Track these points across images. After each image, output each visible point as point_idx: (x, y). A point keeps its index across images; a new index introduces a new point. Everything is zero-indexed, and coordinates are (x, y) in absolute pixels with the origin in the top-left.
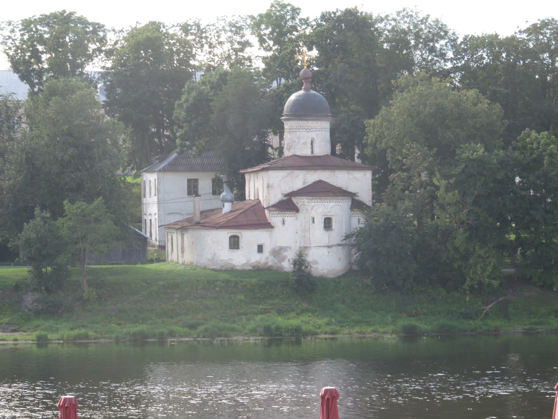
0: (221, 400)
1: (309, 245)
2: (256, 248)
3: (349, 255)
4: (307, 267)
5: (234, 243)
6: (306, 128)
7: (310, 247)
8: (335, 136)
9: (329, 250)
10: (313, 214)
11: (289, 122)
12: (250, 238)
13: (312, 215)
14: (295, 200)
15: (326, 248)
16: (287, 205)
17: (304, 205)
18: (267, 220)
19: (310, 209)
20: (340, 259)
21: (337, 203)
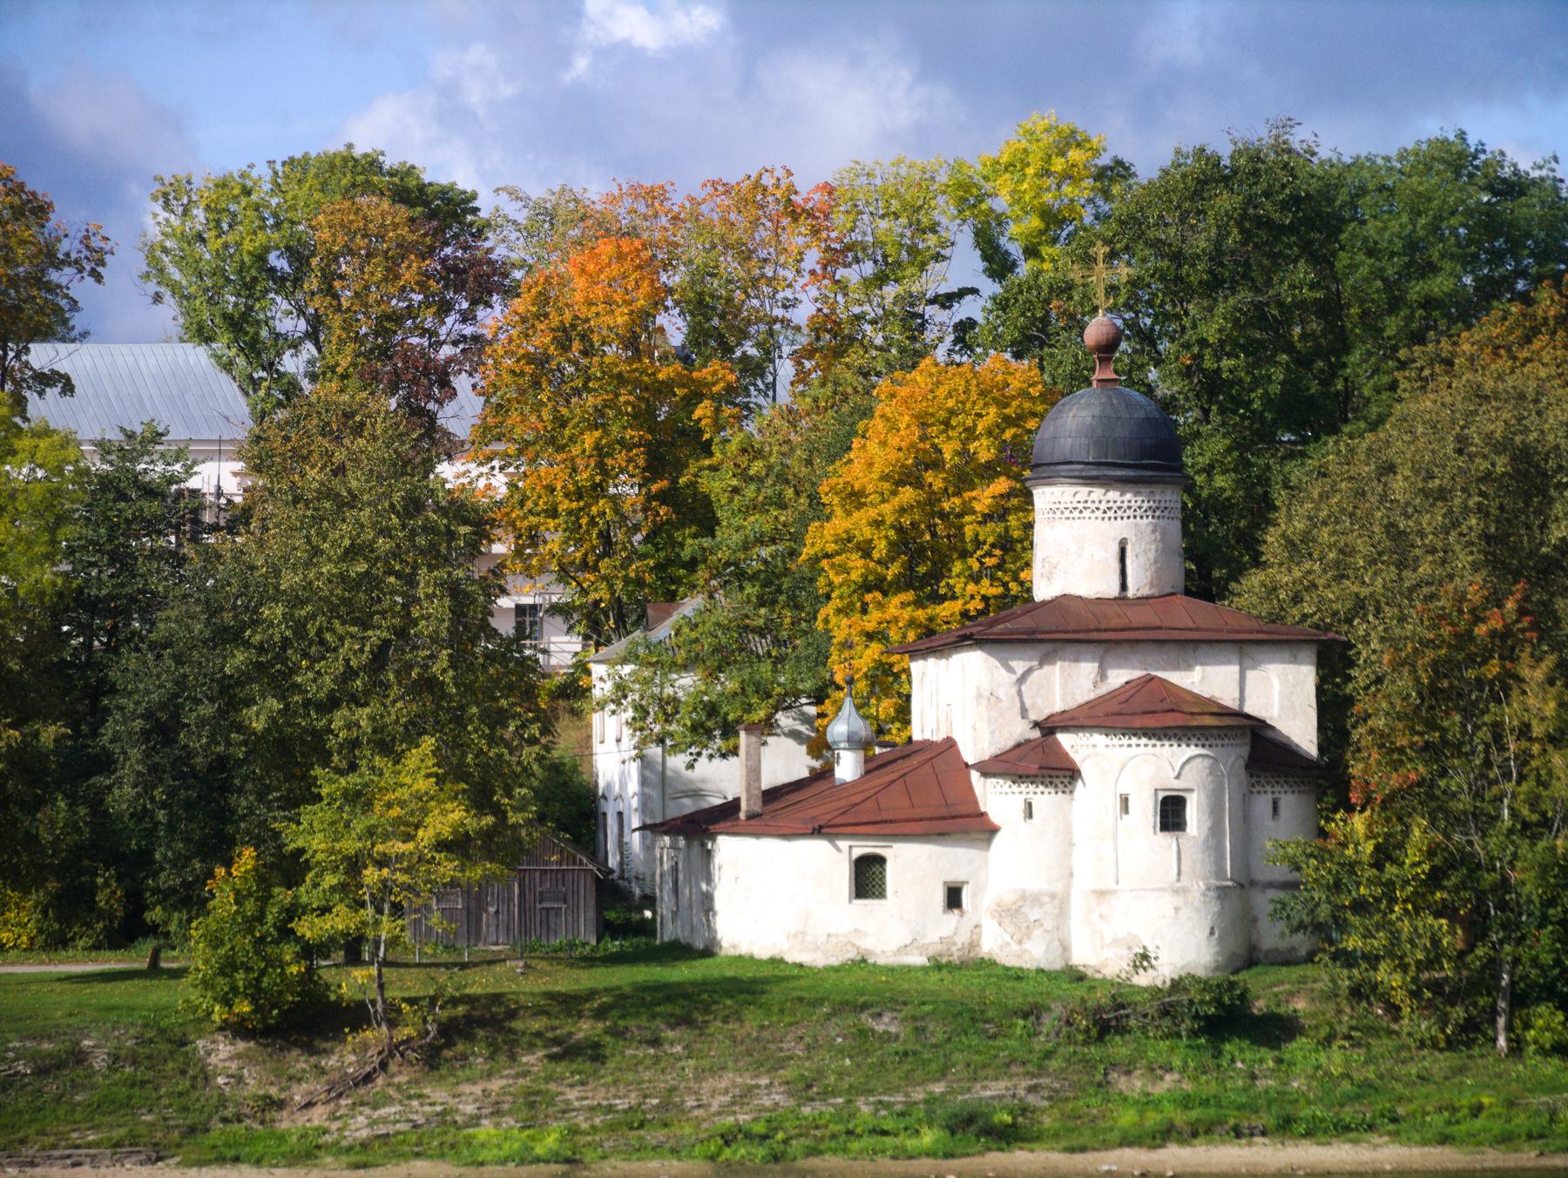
1: (1113, 886)
2: (940, 896)
5: (868, 878)
7: (1115, 891)
11: (1048, 490)
12: (913, 865)
14: (1065, 739)
16: (1040, 762)
18: (976, 803)
20: (1212, 933)
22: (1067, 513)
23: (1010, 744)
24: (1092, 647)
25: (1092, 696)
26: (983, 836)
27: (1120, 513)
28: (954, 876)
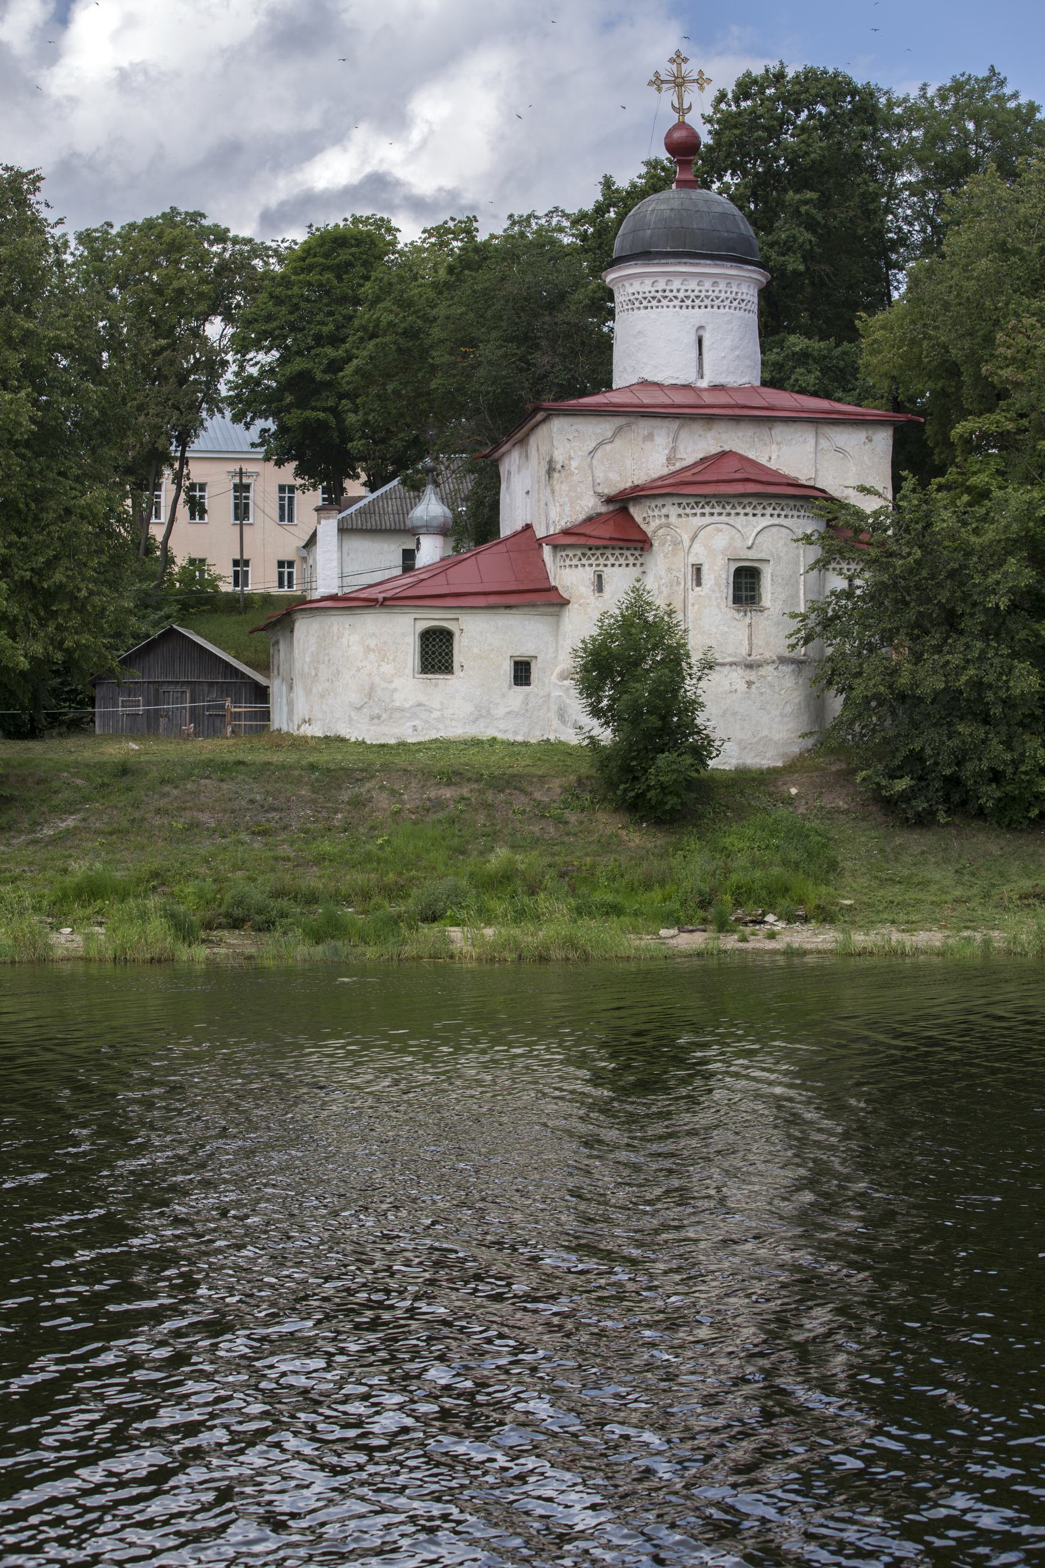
0: (178, 1237)
2: (507, 669)
3: (816, 707)
4: (611, 636)
5: (436, 653)
6: (681, 295)
8: (774, 317)
9: (752, 675)
10: (698, 553)
13: (692, 560)
15: (740, 671)
17: (668, 526)
19: (686, 538)
21: (776, 521)
22: (645, 303)
23: (582, 517)
24: (666, 423)
25: (665, 471)
26: (556, 609)
27: (697, 302)
28: (524, 650)
